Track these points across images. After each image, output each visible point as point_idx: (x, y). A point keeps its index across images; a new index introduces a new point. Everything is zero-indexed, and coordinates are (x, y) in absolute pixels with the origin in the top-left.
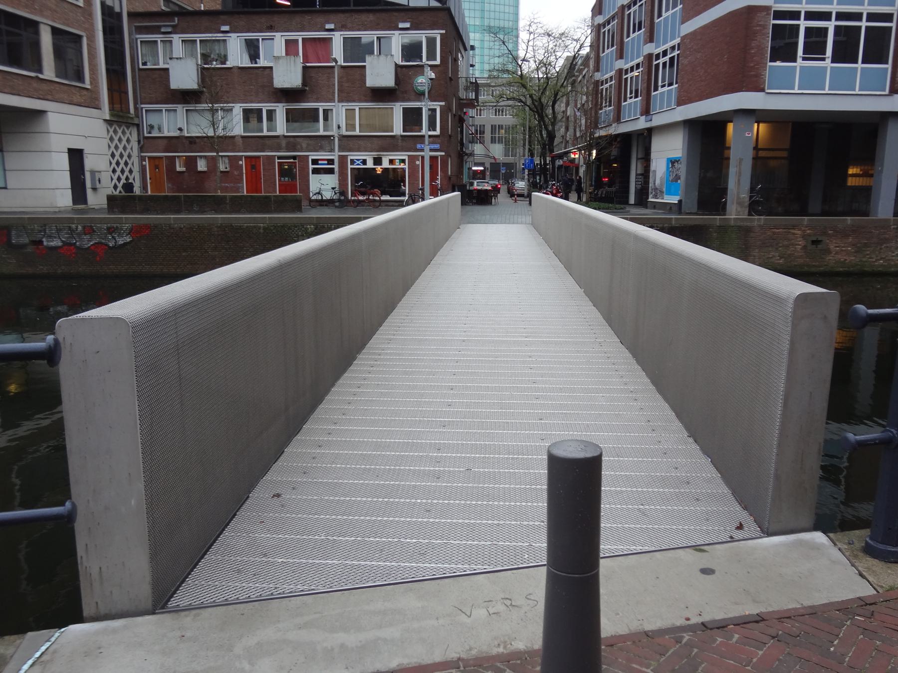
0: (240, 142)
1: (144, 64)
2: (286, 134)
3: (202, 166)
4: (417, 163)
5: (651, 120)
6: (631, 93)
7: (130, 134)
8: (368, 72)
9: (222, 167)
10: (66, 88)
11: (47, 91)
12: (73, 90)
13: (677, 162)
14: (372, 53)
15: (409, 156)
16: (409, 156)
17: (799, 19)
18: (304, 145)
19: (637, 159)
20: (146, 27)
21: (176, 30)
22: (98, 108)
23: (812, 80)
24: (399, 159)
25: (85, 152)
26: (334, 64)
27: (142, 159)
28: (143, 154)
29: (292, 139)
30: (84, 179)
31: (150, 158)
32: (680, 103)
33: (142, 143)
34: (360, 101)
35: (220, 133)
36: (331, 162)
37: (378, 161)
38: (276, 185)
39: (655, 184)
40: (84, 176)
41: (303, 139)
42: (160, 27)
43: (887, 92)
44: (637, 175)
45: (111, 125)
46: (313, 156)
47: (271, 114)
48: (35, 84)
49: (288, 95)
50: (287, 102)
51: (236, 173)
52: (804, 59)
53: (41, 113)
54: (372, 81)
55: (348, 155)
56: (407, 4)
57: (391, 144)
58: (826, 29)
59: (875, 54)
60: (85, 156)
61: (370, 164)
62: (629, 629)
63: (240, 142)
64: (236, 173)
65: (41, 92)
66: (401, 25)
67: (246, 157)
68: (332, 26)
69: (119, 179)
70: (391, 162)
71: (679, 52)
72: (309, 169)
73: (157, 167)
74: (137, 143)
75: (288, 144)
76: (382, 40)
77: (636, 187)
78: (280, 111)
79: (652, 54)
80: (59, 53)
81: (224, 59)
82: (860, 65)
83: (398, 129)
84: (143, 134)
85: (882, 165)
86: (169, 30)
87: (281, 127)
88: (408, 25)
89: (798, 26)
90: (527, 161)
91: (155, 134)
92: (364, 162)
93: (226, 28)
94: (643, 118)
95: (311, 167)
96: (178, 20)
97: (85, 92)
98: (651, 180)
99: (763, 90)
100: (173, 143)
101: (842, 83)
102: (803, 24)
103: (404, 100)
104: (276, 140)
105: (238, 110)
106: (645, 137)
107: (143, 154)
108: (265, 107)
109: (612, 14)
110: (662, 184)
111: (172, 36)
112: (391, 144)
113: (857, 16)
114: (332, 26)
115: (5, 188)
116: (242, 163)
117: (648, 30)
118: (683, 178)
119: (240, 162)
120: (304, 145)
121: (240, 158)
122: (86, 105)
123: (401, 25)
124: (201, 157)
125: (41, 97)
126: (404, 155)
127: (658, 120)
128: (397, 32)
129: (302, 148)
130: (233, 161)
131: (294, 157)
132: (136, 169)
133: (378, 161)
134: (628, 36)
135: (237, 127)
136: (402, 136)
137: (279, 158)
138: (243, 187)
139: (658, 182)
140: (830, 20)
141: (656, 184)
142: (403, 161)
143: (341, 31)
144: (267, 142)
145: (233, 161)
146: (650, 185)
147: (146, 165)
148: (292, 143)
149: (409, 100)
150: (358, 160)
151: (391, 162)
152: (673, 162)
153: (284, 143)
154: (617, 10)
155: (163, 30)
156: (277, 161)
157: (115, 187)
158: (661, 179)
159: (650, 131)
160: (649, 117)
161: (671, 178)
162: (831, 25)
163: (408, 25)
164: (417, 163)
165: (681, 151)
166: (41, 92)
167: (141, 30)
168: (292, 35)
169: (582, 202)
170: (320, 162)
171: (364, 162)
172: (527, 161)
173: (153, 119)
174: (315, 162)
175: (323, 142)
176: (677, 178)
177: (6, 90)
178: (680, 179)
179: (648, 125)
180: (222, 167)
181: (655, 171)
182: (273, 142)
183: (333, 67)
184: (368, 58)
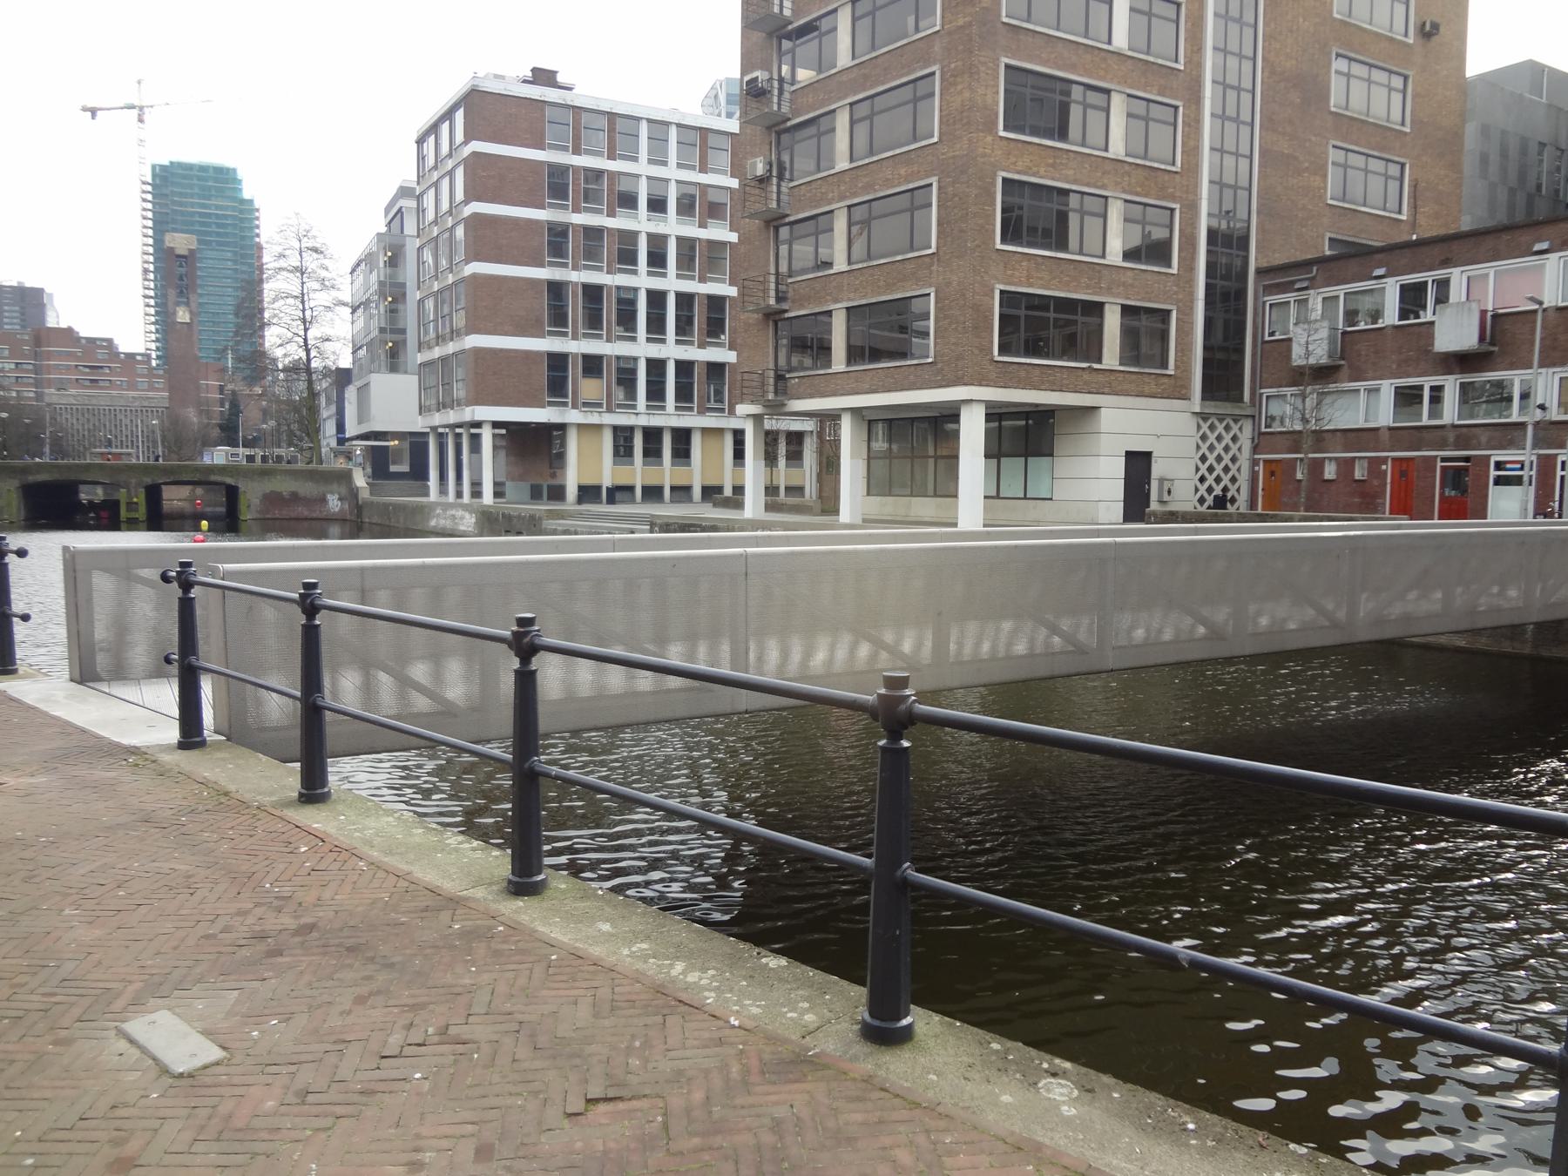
0: (1385, 436)
1: (1272, 334)
2: (1457, 422)
3: (1330, 472)
7: (1240, 429)
9: (1358, 475)
10: (1134, 377)
11: (1111, 384)
12: (1146, 379)
18: (1484, 439)
20: (1278, 285)
21: (1313, 284)
22: (1186, 397)
25: (1154, 455)
26: (1536, 307)
27: (1255, 463)
28: (1256, 456)
29: (1465, 430)
30: (1149, 490)
31: (1266, 461)
33: (1256, 441)
35: (1312, 426)
36: (1522, 464)
38: (1433, 501)
40: (1149, 486)
41: (1482, 428)
42: (1293, 282)
45: (1205, 419)
46: (1497, 456)
47: (1437, 392)
48: (1086, 376)
49: (1462, 361)
50: (1462, 372)
51: (1376, 482)
53: (1094, 409)
54: (1298, 357)
55: (1557, 455)
60: (1153, 460)
62: (547, 736)
63: (1385, 436)
64: (1376, 482)
65: (1094, 385)
67: (1395, 460)
68: (1544, 246)
69: (1210, 490)
72: (1488, 477)
73: (1273, 473)
74: (1250, 441)
75: (1458, 437)
78: (1451, 385)
80: (1130, 336)
81: (1376, 315)
84: (1259, 428)
86: (1305, 284)
87: (1450, 412)
91: (1276, 428)
93: (1380, 272)
95: (1493, 473)
96: (1317, 270)
97: (1166, 380)
100: (1294, 440)
104: (1440, 433)
105: (1387, 388)
107: (1256, 456)
108: (1427, 382)
111: (1384, 280)
114: (1544, 246)
115: (1051, 499)
119: (1384, 467)
120: (1484, 439)
121: (1384, 460)
122: (1165, 395)
124: (1330, 459)
125: (1094, 390)
129: (1479, 444)
130: (1374, 464)
131: (1467, 459)
132: (1245, 474)
135: (1384, 413)
137: (1444, 459)
138: (1384, 504)
143: (1561, 250)
145: (1374, 464)
147: (1258, 471)
148: (1463, 436)
153: (1451, 437)
155: (1297, 286)
156: (1439, 464)
157: (1202, 500)
166: (1094, 385)
167: (1270, 290)
168: (1330, 291)
169: (148, 480)
170: (1508, 466)
173: (1275, 409)
174: (1499, 466)
175: (1510, 434)
177: (1043, 387)
180: (1358, 475)
182: (1435, 435)
183: (1535, 312)
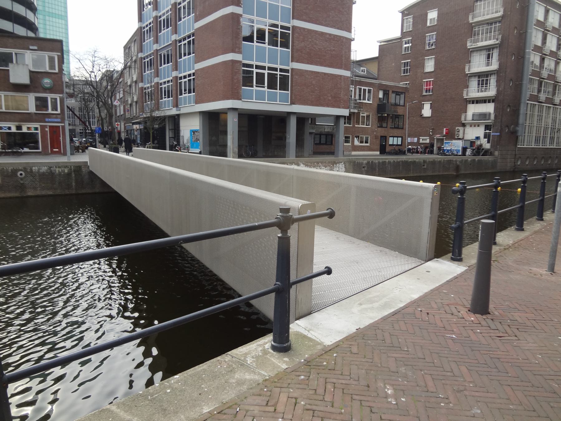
4: (46, 129)
5: (180, 110)
6: (165, 95)
8: (11, 73)
13: (197, 132)
14: (12, 62)
15: (41, 126)
16: (41, 126)
17: (253, 68)
19: (169, 130)
23: (260, 96)
24: (34, 127)
32: (197, 102)
34: (5, 91)
37: (19, 128)
39: (183, 142)
43: (289, 104)
44: (169, 138)
52: (256, 86)
56: (12, 31)
57: (28, 118)
58: (256, 73)
59: (284, 87)
61: (14, 130)
66: (31, 47)
70: (29, 128)
71: (172, 83)
76: (17, 55)
77: (169, 144)
79: (178, 77)
82: (278, 91)
83: (32, 109)
85: (289, 135)
88: (36, 48)
89: (253, 71)
90: (97, 129)
92: (9, 128)
94: (175, 109)
98: (181, 141)
99: (241, 100)
101: (272, 98)
102: (255, 71)
103: (35, 92)
106: (175, 120)
109: (149, 53)
110: (188, 142)
112: (28, 118)
113: (276, 69)
116: (47, 129)
117: (175, 64)
118: (201, 140)
121: (46, 126)
123: (31, 47)
126: (37, 125)
127: (183, 111)
128: (28, 51)
133: (19, 128)
134: (145, 72)
136: (35, 113)
139: (185, 142)
140: (265, 70)
141: (185, 143)
142: (36, 129)
144: (51, 116)
146: (181, 143)
149: (39, 92)
150: (5, 127)
151: (29, 128)
152: (194, 132)
154: (152, 51)
158: (187, 140)
159: (178, 115)
160: (179, 109)
161: (193, 140)
162: (266, 72)
163: (36, 48)
164: (46, 129)
165: (199, 127)
171: (9, 128)
172: (97, 129)
176: (197, 140)
178: (199, 140)
179: (178, 113)
181: (183, 137)
184: (10, 65)
